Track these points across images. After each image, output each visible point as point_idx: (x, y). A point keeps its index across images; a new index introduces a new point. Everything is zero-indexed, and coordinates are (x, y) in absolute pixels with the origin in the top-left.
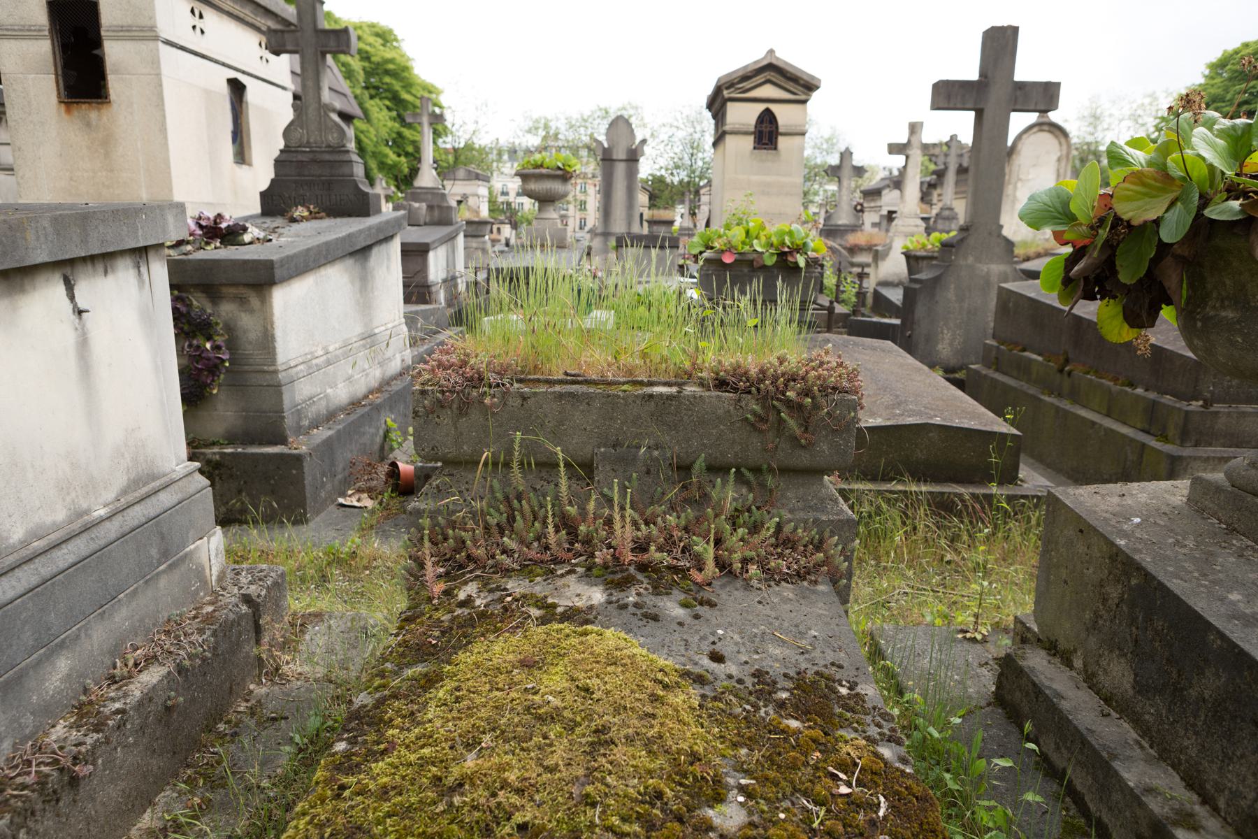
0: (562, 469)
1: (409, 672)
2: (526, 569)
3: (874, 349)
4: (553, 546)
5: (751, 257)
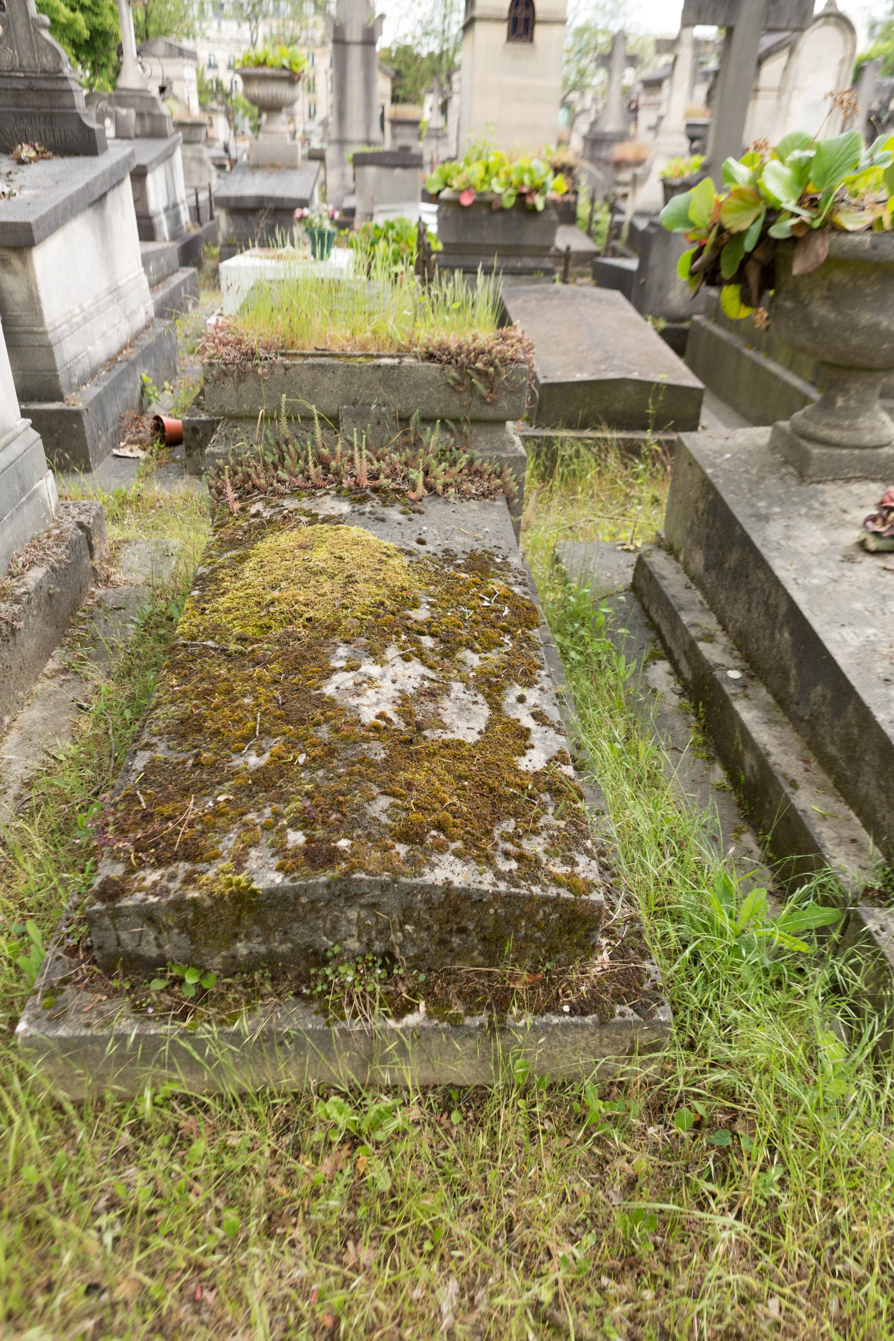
0: (317, 421)
1: (229, 554)
2: (295, 493)
3: (600, 301)
4: (313, 477)
5: (489, 198)
